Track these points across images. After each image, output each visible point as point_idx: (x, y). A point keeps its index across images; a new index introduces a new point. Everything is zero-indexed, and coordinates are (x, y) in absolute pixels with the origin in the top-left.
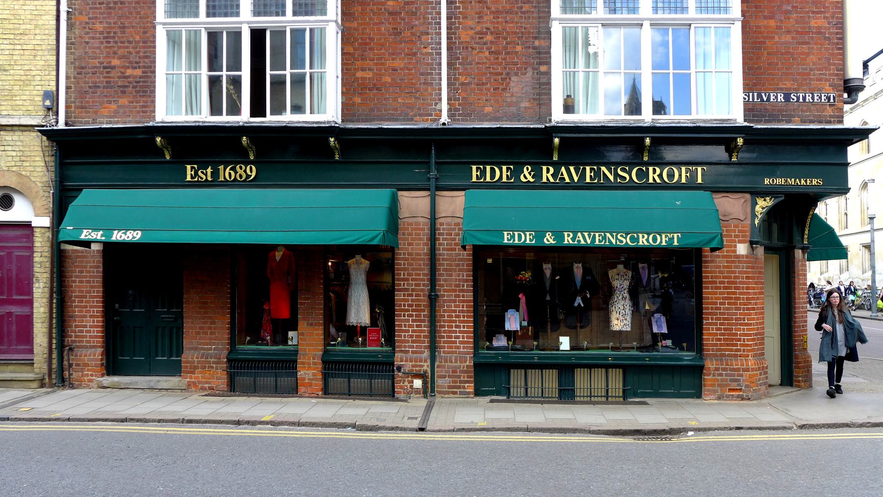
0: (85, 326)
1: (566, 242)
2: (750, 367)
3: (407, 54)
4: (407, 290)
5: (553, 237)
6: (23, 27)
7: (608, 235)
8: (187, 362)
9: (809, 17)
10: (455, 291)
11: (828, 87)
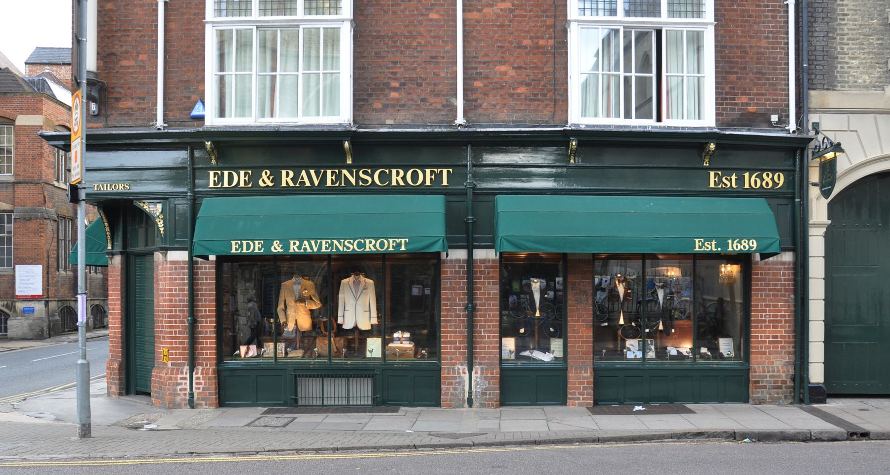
1: (291, 250)
5: (281, 246)
7: (335, 242)
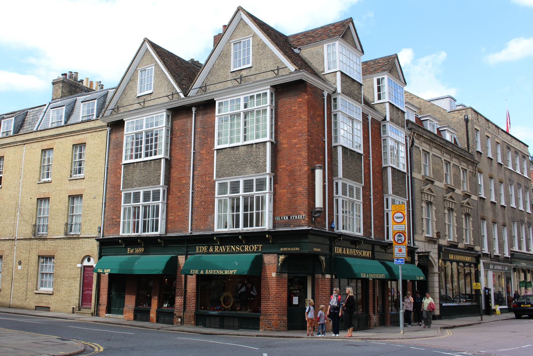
0: (103, 298)
3: (182, 210)
4: (179, 288)
6: (95, 208)
8: (125, 310)
10: (191, 289)
11: (302, 213)
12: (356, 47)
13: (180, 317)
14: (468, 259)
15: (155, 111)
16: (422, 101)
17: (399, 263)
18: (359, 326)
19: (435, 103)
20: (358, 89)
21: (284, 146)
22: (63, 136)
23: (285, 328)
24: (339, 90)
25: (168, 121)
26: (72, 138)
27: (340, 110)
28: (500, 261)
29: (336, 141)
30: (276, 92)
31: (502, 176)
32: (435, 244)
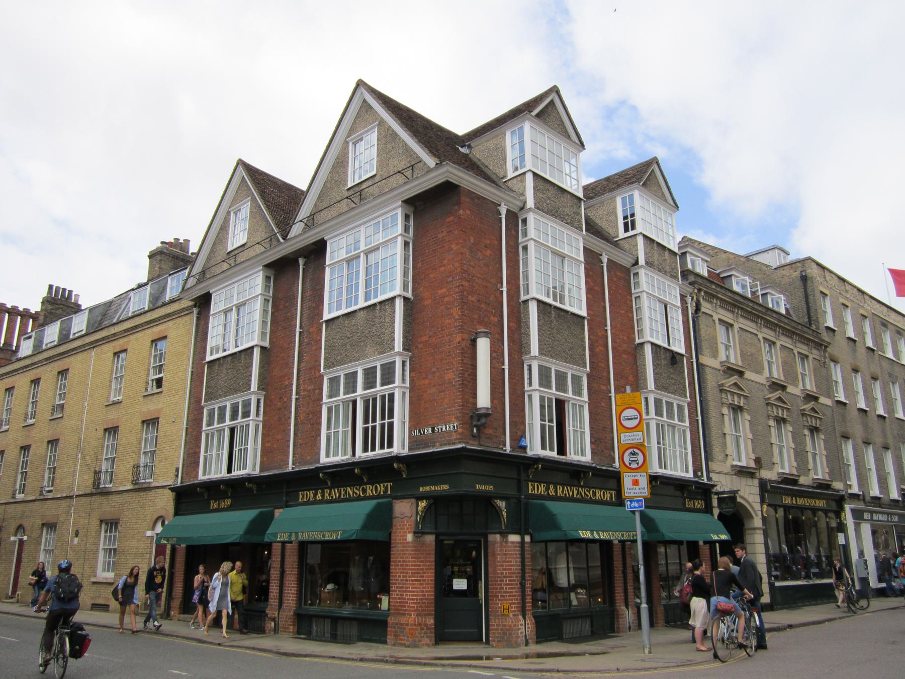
2: (410, 623)
9: (445, 373)
12: (569, 137)
13: (274, 620)
14: (820, 503)
15: (246, 272)
16: (732, 256)
17: (635, 507)
18: (592, 632)
19: (756, 258)
20: (572, 206)
21: (426, 303)
22: (140, 329)
23: (430, 640)
24: (530, 203)
25: (267, 287)
26: (150, 330)
27: (533, 237)
28: (883, 506)
29: (527, 292)
30: (415, 213)
31: (875, 369)
32: (752, 478)
